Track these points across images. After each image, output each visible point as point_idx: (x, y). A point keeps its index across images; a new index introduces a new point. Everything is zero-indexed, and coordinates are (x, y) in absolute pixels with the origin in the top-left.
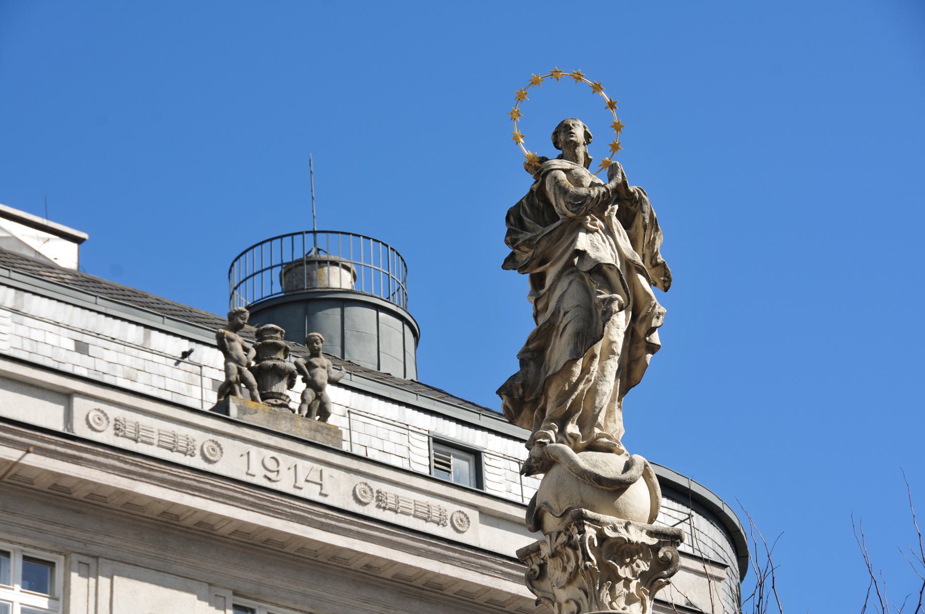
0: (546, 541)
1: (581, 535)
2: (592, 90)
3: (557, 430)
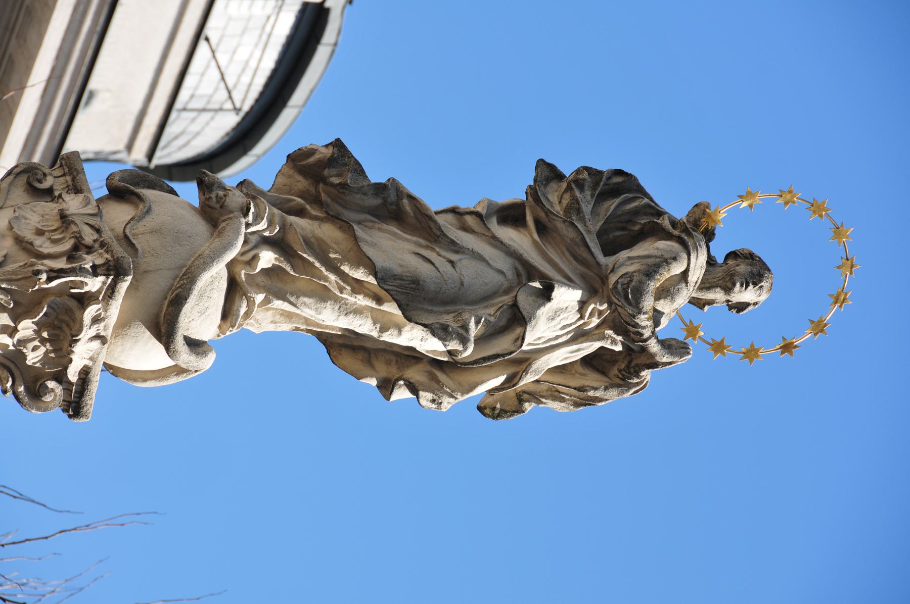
0: (90, 206)
1: (90, 270)
2: (816, 320)
3: (267, 234)
